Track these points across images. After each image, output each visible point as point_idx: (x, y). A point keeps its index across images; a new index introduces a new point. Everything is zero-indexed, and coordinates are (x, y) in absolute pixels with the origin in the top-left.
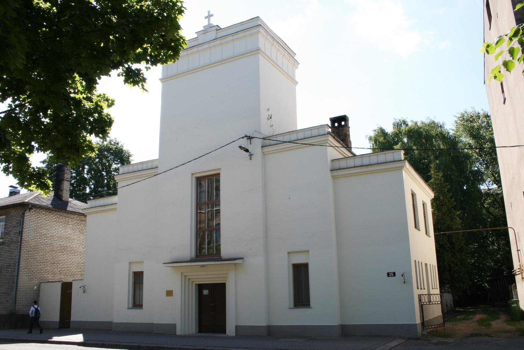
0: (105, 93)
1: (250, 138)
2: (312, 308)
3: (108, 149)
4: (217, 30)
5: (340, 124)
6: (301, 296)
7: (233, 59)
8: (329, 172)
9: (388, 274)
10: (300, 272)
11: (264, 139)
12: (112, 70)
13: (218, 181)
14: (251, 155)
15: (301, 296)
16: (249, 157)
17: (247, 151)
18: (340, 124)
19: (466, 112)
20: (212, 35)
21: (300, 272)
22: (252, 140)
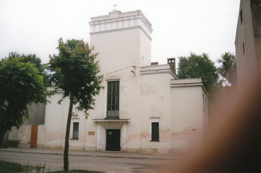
0: (58, 40)
1: (135, 67)
2: (160, 141)
3: (87, 63)
4: (119, 13)
5: (171, 61)
6: (155, 137)
7: (126, 29)
8: (170, 85)
9: (193, 130)
10: (155, 126)
11: (141, 68)
12: (187, 57)
13: (93, 135)
14: (135, 74)
15: (155, 137)
16: (134, 75)
17: (134, 72)
18: (171, 61)
19: (217, 60)
20: (116, 16)
21: (155, 126)
22: (136, 68)
